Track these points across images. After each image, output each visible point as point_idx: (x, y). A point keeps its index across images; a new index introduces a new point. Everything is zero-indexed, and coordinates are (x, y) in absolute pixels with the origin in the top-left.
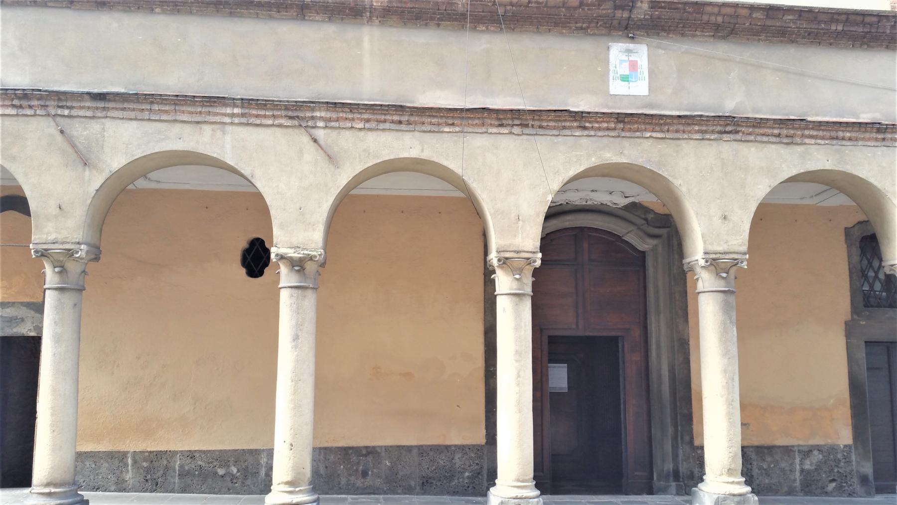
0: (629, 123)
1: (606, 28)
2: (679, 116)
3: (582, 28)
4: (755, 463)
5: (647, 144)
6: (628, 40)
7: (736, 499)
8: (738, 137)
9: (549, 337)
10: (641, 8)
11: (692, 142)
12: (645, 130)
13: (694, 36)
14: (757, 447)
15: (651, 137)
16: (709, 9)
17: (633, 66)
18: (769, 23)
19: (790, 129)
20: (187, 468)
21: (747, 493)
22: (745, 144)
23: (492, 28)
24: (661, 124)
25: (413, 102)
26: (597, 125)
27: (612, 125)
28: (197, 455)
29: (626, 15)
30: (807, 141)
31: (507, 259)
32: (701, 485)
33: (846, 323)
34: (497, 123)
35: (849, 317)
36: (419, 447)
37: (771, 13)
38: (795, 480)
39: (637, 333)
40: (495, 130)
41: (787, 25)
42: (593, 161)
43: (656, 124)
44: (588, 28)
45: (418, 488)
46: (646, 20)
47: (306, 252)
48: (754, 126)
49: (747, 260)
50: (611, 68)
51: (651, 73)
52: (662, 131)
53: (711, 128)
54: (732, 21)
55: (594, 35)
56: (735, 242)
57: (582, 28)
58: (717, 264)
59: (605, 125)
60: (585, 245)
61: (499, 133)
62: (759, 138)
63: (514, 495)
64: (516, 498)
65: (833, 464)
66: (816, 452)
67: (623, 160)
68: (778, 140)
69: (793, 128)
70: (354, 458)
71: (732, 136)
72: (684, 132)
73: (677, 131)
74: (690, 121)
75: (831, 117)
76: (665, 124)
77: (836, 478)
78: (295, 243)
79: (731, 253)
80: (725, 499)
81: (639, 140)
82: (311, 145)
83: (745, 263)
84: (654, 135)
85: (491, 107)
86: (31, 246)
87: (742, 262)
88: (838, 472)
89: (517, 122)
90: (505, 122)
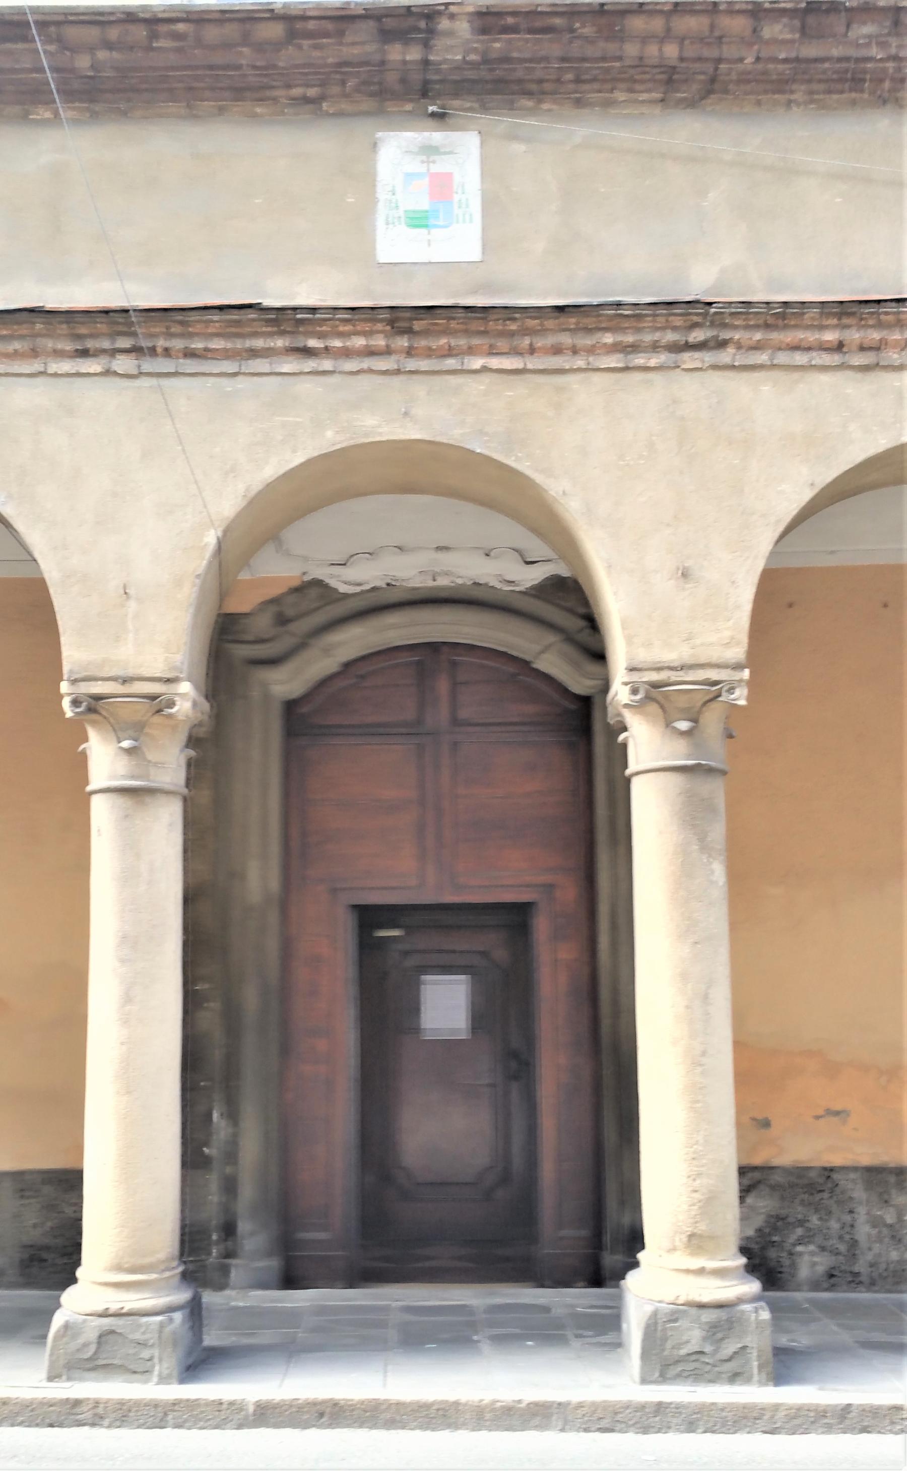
0: (426, 333)
1: (372, 95)
2: (560, 309)
3: (306, 100)
4: (862, 1211)
5: (476, 387)
6: (431, 122)
7: (708, 1316)
8: (726, 356)
10: (450, 33)
11: (596, 377)
12: (471, 351)
13: (609, 104)
14: (869, 1170)
15: (485, 369)
16: (637, 23)
17: (442, 187)
18: (811, 50)
21: (740, 1300)
22: (745, 375)
24: (512, 334)
26: (337, 343)
27: (380, 342)
29: (414, 54)
31: (98, 698)
32: (622, 1282)
34: (69, 346)
37: (811, 20)
39: (569, 893)
40: (66, 366)
41: (863, 53)
42: (330, 439)
43: (502, 334)
44: (322, 98)
46: (474, 65)
48: (767, 326)
50: (382, 195)
52: (515, 352)
53: (648, 338)
54: (707, 53)
55: (340, 114)
57: (306, 100)
58: (666, 695)
59: (359, 342)
60: (443, 686)
61: (78, 375)
62: (783, 358)
63: (100, 1308)
64: (105, 1314)
67: (414, 433)
68: (835, 359)
69: (880, 325)
71: (708, 357)
72: (575, 351)
73: (557, 350)
74: (589, 322)
76: (526, 332)
79: (702, 666)
80: (674, 1317)
81: (453, 380)
84: (495, 362)
85: (50, 305)
86: (64, 687)
87: (731, 690)
89: (124, 343)
90: (90, 344)
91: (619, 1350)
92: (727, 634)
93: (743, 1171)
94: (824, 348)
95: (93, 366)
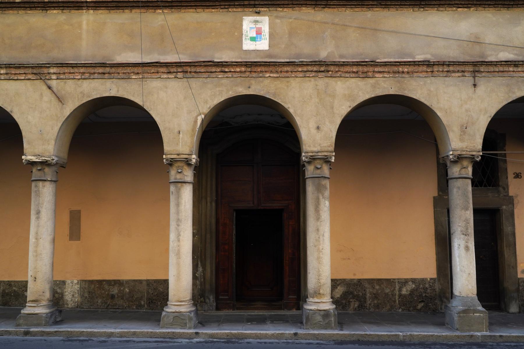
4: (368, 290)
5: (267, 82)
6: (256, 14)
9: (79, 212)
17: (259, 32)
19: (364, 67)
20: (7, 291)
22: (334, 79)
23: (166, 11)
25: (113, 60)
28: (13, 284)
30: (377, 75)
33: (434, 198)
35: (436, 194)
36: (147, 281)
38: (395, 301)
40: (165, 76)
42: (231, 94)
45: (146, 306)
47: (43, 158)
49: (481, 156)
50: (244, 33)
51: (271, 35)
56: (325, 145)
65: (422, 290)
66: (410, 283)
68: (356, 75)
70: (106, 287)
75: (394, 58)
77: (424, 300)
78: (37, 153)
79: (323, 152)
82: (47, 92)
83: (333, 158)
84: (272, 75)
86: (164, 156)
88: (426, 296)
91: (68, 238)
92: (329, 144)
93: (332, 280)
94: (354, 72)
95: (171, 76)
